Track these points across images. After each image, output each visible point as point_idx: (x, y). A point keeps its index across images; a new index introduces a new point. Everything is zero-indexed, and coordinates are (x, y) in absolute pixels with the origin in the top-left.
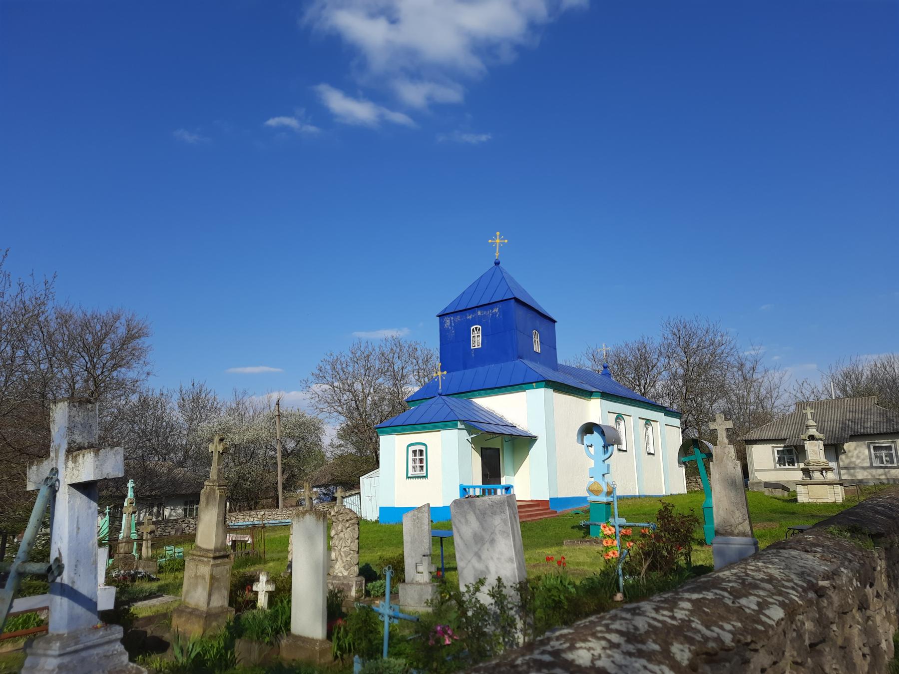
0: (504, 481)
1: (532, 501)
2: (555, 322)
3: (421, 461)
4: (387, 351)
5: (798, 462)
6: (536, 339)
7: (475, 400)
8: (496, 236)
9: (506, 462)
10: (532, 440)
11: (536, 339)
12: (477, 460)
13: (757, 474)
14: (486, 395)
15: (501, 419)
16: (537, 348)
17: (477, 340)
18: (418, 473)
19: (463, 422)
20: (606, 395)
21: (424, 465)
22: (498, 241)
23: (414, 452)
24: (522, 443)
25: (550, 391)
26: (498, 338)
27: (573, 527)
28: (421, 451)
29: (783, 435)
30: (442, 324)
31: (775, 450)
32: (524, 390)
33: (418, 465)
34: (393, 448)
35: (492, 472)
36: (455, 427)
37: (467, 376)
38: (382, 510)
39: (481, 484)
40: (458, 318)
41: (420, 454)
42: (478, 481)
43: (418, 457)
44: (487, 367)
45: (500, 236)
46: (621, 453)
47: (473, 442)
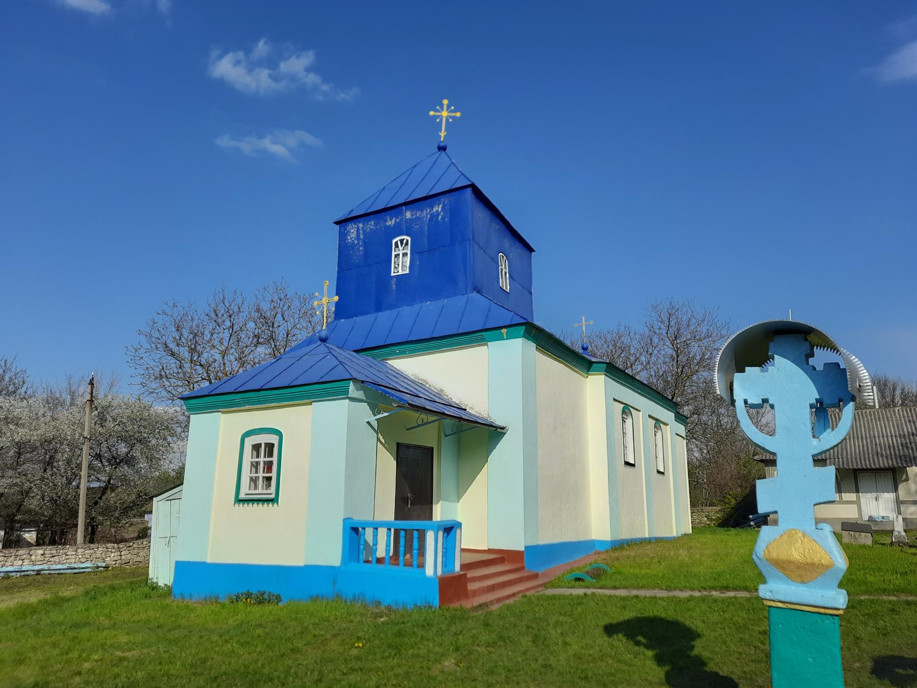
0: (440, 512)
1: (490, 551)
2: (531, 250)
3: (269, 466)
6: (504, 267)
8: (442, 106)
9: (443, 471)
10: (494, 433)
11: (504, 267)
12: (388, 465)
15: (439, 394)
16: (505, 283)
17: (401, 263)
18: (261, 491)
19: (361, 383)
20: (614, 371)
22: (445, 114)
23: (256, 447)
24: (476, 436)
25: (532, 346)
26: (439, 259)
27: (610, 630)
28: (270, 446)
30: (343, 236)
32: (482, 342)
33: (261, 474)
34: (214, 442)
35: (415, 490)
36: (342, 394)
37: (382, 323)
38: (182, 568)
40: (371, 225)
41: (266, 454)
42: (387, 510)
43: (262, 459)
44: (417, 306)
45: (449, 106)
46: (629, 469)
47: (382, 428)
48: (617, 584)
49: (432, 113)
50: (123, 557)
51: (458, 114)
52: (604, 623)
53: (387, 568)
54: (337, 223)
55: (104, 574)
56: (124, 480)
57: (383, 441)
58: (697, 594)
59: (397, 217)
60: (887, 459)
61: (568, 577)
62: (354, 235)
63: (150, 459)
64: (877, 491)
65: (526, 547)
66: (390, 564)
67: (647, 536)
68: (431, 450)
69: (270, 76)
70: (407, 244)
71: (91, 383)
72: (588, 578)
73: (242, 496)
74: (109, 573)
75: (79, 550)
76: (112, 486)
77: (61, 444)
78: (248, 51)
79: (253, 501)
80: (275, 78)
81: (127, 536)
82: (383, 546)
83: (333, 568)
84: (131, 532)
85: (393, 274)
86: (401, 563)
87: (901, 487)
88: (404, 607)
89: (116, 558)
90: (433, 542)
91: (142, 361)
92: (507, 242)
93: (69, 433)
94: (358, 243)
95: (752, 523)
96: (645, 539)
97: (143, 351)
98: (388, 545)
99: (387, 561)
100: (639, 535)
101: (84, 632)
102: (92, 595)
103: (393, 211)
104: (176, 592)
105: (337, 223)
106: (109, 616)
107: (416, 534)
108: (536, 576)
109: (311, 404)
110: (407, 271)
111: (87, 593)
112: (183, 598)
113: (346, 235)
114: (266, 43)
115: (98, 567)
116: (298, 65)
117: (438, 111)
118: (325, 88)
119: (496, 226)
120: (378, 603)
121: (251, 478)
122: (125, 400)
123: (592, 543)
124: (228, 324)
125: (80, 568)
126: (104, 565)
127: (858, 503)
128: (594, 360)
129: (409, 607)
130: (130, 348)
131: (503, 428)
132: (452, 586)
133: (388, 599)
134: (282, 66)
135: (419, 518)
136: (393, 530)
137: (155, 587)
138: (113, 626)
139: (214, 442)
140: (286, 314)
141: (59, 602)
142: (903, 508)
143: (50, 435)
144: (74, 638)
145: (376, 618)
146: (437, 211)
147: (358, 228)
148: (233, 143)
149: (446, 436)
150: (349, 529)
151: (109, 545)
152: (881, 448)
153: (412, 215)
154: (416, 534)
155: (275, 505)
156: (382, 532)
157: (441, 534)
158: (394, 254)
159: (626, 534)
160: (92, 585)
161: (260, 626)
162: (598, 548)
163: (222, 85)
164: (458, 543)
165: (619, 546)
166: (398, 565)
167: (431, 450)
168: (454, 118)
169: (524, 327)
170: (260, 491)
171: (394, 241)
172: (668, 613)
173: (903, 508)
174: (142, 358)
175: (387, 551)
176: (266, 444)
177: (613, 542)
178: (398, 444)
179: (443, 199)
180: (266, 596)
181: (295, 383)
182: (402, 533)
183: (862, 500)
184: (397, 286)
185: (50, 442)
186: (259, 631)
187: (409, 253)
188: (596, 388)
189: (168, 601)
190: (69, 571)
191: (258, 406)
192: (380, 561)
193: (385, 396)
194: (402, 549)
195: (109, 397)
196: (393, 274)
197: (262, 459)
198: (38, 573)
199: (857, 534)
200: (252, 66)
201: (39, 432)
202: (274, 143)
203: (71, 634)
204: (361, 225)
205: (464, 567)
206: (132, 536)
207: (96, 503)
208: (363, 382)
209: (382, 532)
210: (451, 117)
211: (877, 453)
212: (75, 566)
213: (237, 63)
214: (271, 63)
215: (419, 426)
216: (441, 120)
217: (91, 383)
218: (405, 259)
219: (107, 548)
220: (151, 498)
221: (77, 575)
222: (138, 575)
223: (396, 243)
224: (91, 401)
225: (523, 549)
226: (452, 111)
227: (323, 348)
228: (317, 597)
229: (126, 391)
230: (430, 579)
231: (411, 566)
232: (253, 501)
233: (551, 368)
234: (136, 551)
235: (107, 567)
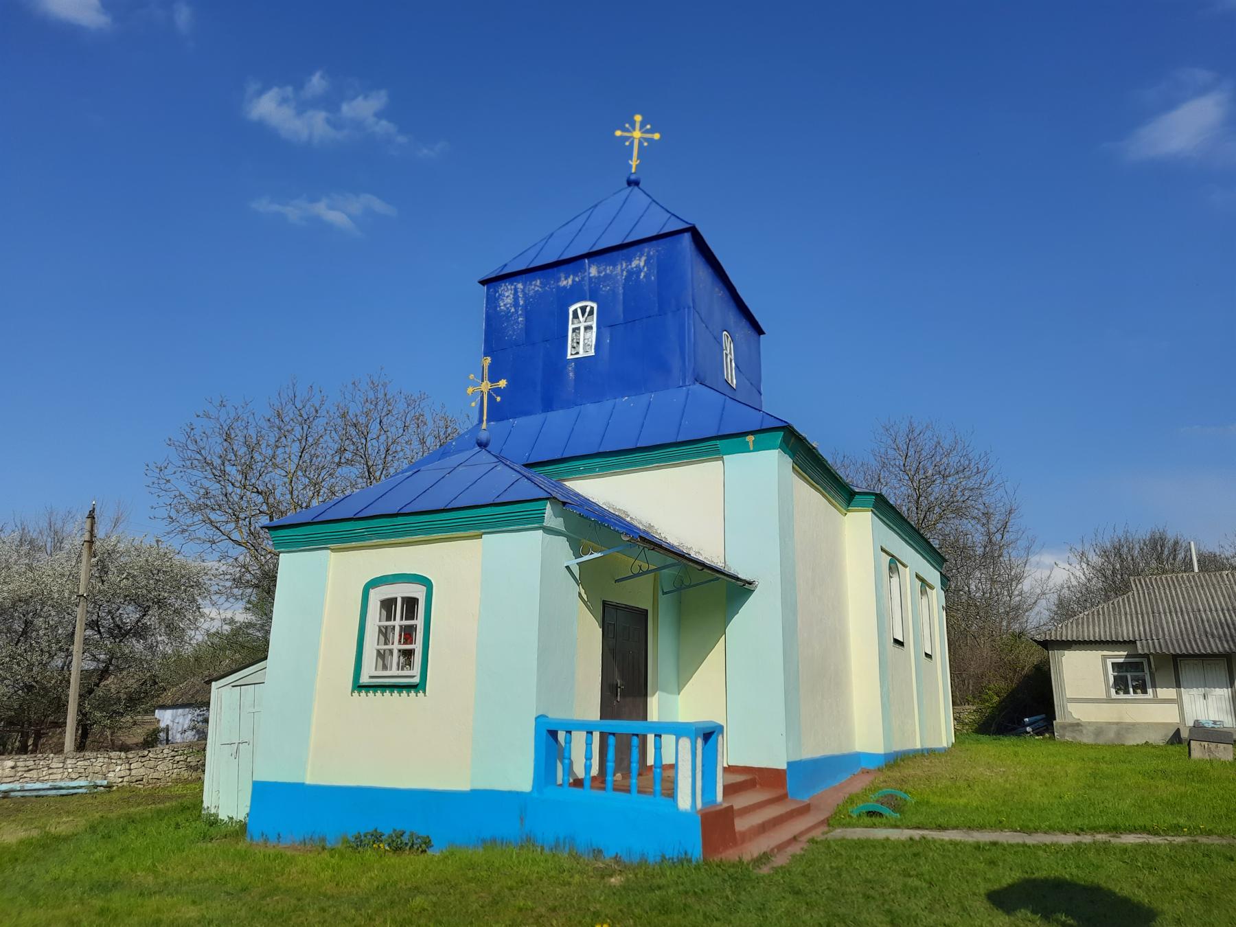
2: (760, 331)
3: (408, 634)
4: (354, 410)
5: (1154, 686)
7: (567, 483)
10: (736, 590)
12: (588, 635)
13: (1071, 707)
14: (606, 470)
18: (394, 672)
20: (884, 508)
21: (418, 647)
22: (637, 134)
23: (388, 605)
24: (709, 593)
25: (788, 461)
26: (611, 350)
27: (1002, 899)
28: (411, 604)
29: (1126, 633)
30: (492, 301)
31: (1109, 662)
32: (716, 454)
33: (396, 647)
36: (535, 521)
38: (262, 792)
39: (592, 712)
40: (536, 285)
41: (405, 615)
43: (398, 622)
44: (608, 404)
46: (898, 649)
47: (587, 577)
48: (941, 821)
49: (618, 133)
50: (133, 772)
51: (657, 136)
52: (983, 888)
53: (587, 794)
54: (483, 282)
55: (107, 797)
56: (129, 659)
57: (585, 597)
58: (1087, 839)
59: (575, 275)
60: (1220, 640)
61: (854, 810)
62: (509, 301)
63: (171, 629)
64: (1205, 686)
65: (789, 764)
66: (592, 787)
67: (918, 746)
68: (644, 613)
69: (328, 121)
70: (591, 313)
72: (886, 811)
73: (365, 680)
74: (115, 796)
75: (69, 761)
76: (100, 672)
77: (43, 604)
78: (299, 86)
79: (383, 687)
80: (335, 125)
81: (130, 741)
82: (582, 755)
83: (518, 794)
84: (138, 735)
85: (569, 357)
86: (609, 785)
88: (643, 861)
89: (123, 774)
90: (689, 757)
91: (169, 485)
92: (732, 316)
93: (55, 589)
94: (516, 311)
95: (1028, 729)
96: (917, 751)
97: (171, 469)
98: (589, 758)
99: (587, 783)
100: (908, 746)
101: (117, 900)
102: (101, 831)
103: (571, 265)
104: (254, 829)
106: (153, 870)
107: (635, 741)
108: (805, 810)
109: (480, 536)
110: (592, 353)
111: (93, 829)
112: (266, 840)
113: (497, 299)
114: (322, 77)
115: (96, 786)
116: (364, 108)
117: (628, 131)
118: (401, 139)
119: (719, 292)
120: (598, 853)
121: (378, 651)
122: (136, 543)
123: (856, 757)
124: (298, 432)
125: (69, 788)
126: (105, 783)
127: (1179, 701)
128: (857, 490)
129: (651, 860)
130: (152, 466)
131: (750, 583)
132: (717, 825)
133: (613, 846)
134: (345, 108)
135: (630, 717)
136: (596, 735)
137: (213, 822)
138: (164, 888)
139: (325, 590)
140: (385, 420)
141: (49, 844)
143: (26, 591)
144: (102, 912)
145: (603, 877)
146: (638, 266)
147: (516, 290)
148: (275, 208)
149: (664, 593)
150: (545, 733)
151: (112, 754)
152: (1210, 626)
153: (599, 272)
154: (635, 741)
155: (421, 694)
156: (579, 737)
157: (700, 742)
158: (571, 327)
159: (899, 746)
160: (97, 815)
161: (417, 889)
162: (864, 765)
163: (263, 133)
164: (719, 758)
165: (896, 760)
166: (604, 789)
167: (644, 613)
168: (650, 140)
169: (782, 434)
170: (394, 672)
171: (571, 309)
172: (1070, 871)
174: (168, 481)
175: (588, 768)
176: (403, 598)
177: (886, 755)
178: (605, 603)
180: (405, 839)
181: (450, 506)
182: (612, 741)
184: (576, 374)
185: (27, 602)
186: (419, 900)
187: (594, 326)
188: (860, 530)
189: (241, 846)
190: (53, 792)
191: (393, 540)
192: (578, 783)
193: (593, 527)
194: (611, 765)
195: (113, 539)
196: (569, 357)
197: (398, 622)
200: (303, 107)
201: (11, 587)
202: (331, 208)
203: (98, 903)
204: (520, 286)
205: (729, 790)
206: (135, 740)
207: (91, 691)
208: (564, 504)
209: (579, 737)
210: (646, 140)
211: (1206, 632)
212: (62, 784)
213: (284, 101)
214: (330, 103)
215: (635, 576)
216: (632, 143)
217: (91, 516)
218: (588, 335)
219: (110, 758)
220: (209, 683)
221: (65, 800)
222: (186, 804)
223: (575, 312)
224: (91, 542)
225: (784, 767)
226: (647, 132)
227: (484, 456)
228: (494, 841)
229: (143, 529)
230: (685, 814)
231: (628, 791)
232: (383, 687)
233: (808, 497)
234: (152, 763)
235: (109, 787)
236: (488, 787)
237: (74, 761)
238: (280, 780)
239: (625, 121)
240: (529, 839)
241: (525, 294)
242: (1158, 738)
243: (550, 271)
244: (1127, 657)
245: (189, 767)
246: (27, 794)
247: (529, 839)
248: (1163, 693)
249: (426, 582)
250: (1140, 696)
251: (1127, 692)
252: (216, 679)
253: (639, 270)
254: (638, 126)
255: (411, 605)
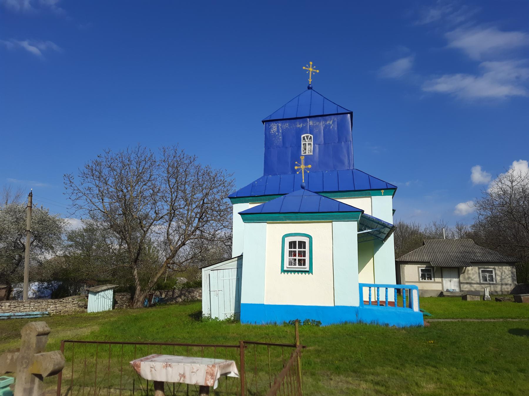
5: (434, 277)
22: (311, 69)
23: (291, 243)
29: (426, 259)
32: (370, 196)
40: (287, 125)
50: (57, 308)
59: (303, 123)
62: (275, 130)
71: (31, 195)
73: (285, 269)
87: (461, 276)
89: (53, 309)
94: (278, 134)
105: (263, 122)
113: (270, 129)
115: (43, 314)
125: (33, 315)
127: (442, 283)
142: (462, 285)
146: (329, 123)
155: (310, 274)
158: (302, 143)
168: (315, 72)
171: (303, 136)
173: (462, 285)
179: (333, 117)
183: (444, 282)
187: (312, 144)
198: (9, 317)
199: (474, 297)
204: (280, 125)
212: (30, 313)
216: (309, 72)
220: (201, 269)
223: (304, 137)
234: (65, 304)
236: (342, 305)
237: (33, 303)
238: (253, 303)
239: (306, 64)
240: (360, 322)
241: (282, 128)
242: (434, 295)
243: (293, 121)
244: (426, 267)
245: (80, 306)
246: (18, 317)
247: (360, 322)
248: (438, 280)
249: (310, 237)
250: (430, 281)
251: (425, 279)
252: (204, 268)
253: (330, 125)
254: (311, 66)
255: (302, 244)
